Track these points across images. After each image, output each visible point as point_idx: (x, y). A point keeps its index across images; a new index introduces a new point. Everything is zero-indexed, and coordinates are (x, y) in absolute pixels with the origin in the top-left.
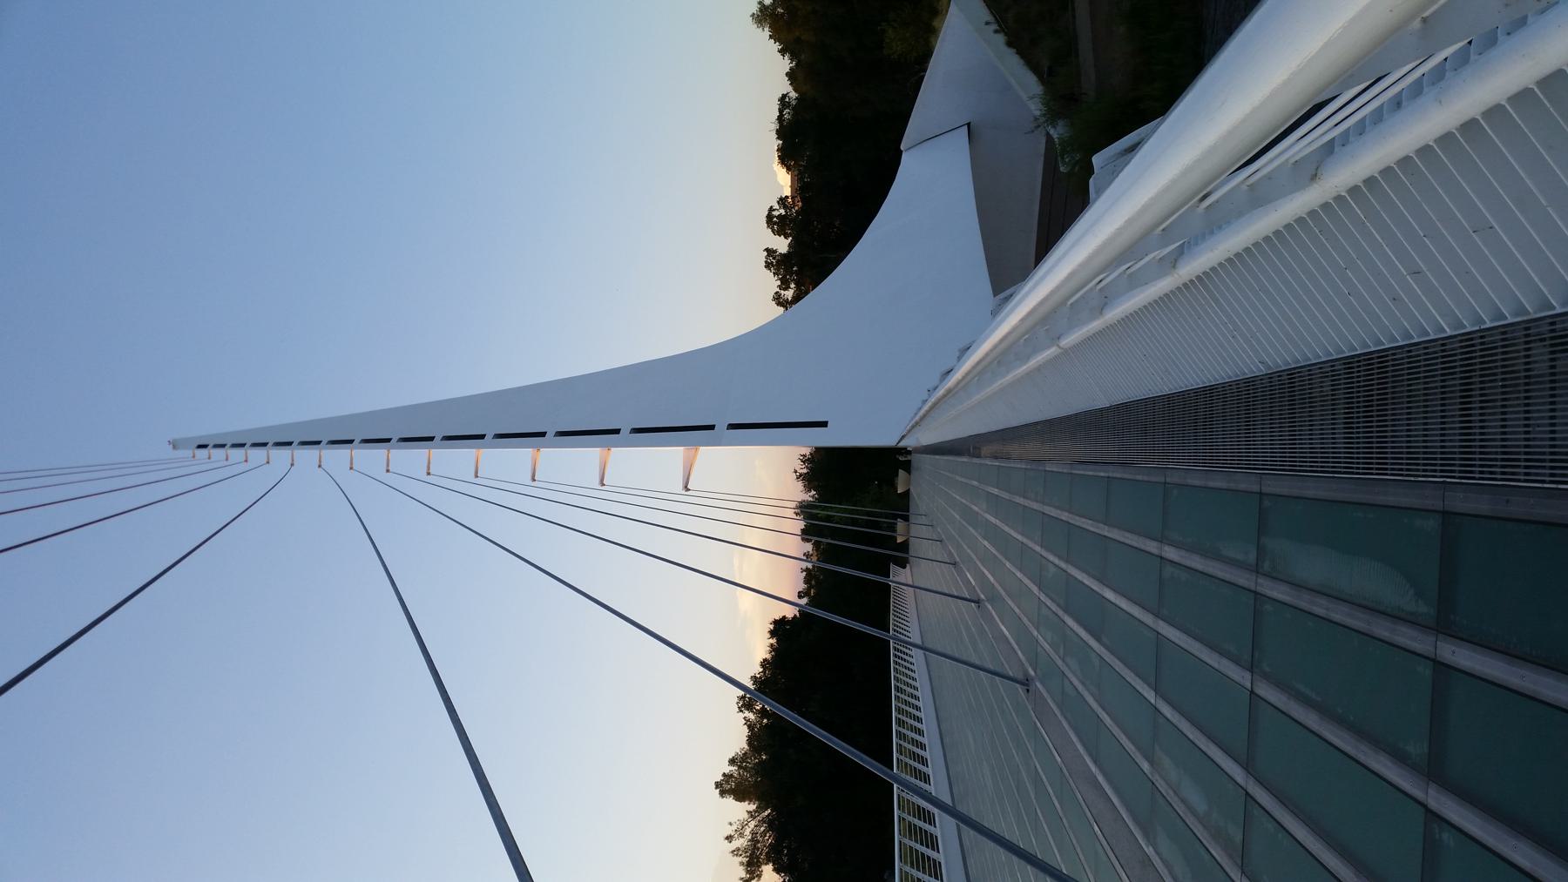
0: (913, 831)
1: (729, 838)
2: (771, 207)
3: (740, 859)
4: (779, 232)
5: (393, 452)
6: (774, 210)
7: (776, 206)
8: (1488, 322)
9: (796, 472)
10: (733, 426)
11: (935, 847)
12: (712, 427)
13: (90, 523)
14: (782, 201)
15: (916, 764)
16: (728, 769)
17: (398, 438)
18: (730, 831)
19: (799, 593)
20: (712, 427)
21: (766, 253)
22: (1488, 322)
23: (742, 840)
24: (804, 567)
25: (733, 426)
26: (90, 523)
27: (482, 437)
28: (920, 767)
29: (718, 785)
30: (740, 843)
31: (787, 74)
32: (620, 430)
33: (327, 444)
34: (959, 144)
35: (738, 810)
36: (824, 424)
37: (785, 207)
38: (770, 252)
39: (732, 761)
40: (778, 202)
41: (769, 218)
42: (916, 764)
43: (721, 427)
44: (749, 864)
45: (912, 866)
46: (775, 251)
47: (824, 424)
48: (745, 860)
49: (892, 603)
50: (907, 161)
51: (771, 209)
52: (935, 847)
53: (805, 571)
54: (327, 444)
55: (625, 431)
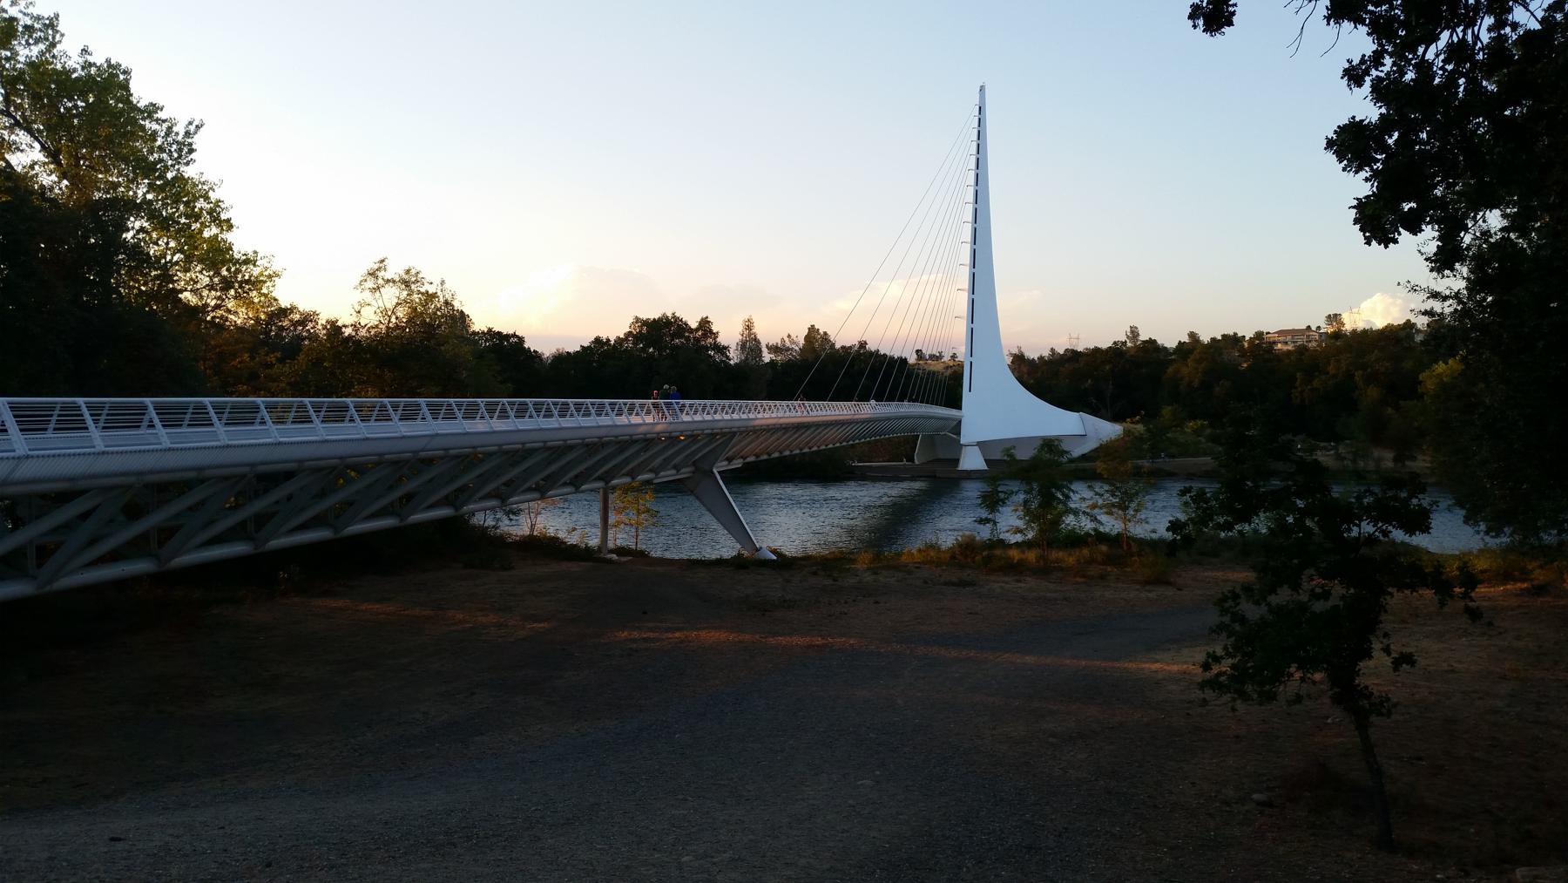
1: (789, 336)
3: (780, 343)
5: (968, 268)
8: (424, 406)
10: (975, 250)
16: (821, 332)
18: (793, 336)
20: (971, 363)
22: (424, 406)
25: (975, 250)
29: (813, 326)
30: (788, 344)
34: (1079, 431)
35: (800, 336)
36: (970, 391)
39: (825, 333)
43: (975, 247)
44: (777, 347)
47: (970, 391)
48: (779, 346)
50: (1075, 415)
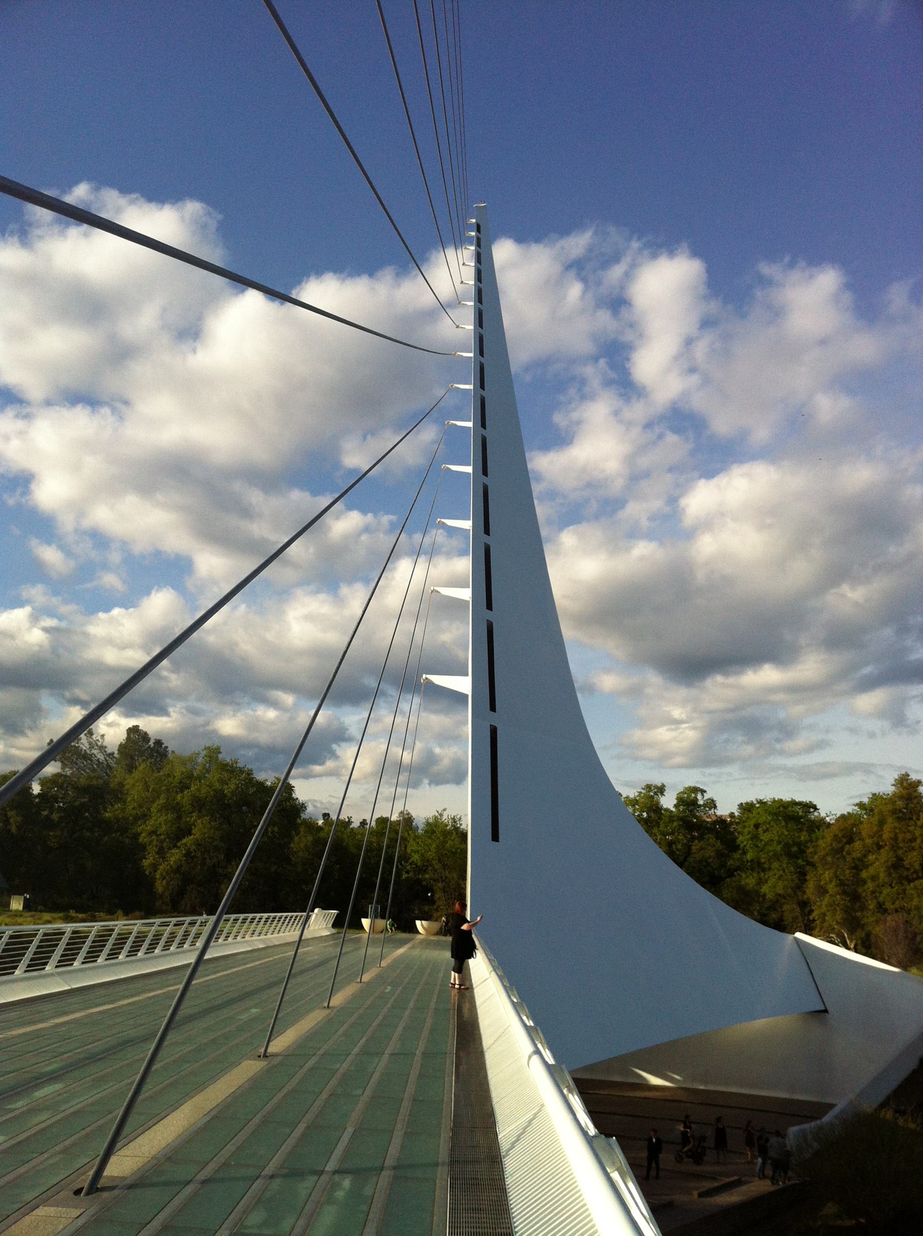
0: (51, 941)
2: (705, 791)
4: (681, 801)
6: (703, 795)
7: (707, 796)
9: (445, 810)
10: (494, 732)
11: (61, 963)
12: (493, 708)
13: (431, 288)
14: (712, 804)
15: (109, 945)
17: (485, 396)
19: (328, 814)
20: (493, 708)
21: (659, 785)
23: (87, 745)
24: (352, 820)
25: (494, 732)
26: (431, 288)
27: (489, 606)
28: (106, 951)
31: (874, 795)
32: (498, 841)
33: (480, 362)
37: (705, 805)
38: (661, 790)
40: (710, 799)
41: (695, 790)
42: (109, 945)
45: (119, 934)
46: (662, 794)
49: (295, 914)
51: (703, 792)
52: (61, 963)
53: (349, 821)
54: (480, 362)
55: (486, 480)
